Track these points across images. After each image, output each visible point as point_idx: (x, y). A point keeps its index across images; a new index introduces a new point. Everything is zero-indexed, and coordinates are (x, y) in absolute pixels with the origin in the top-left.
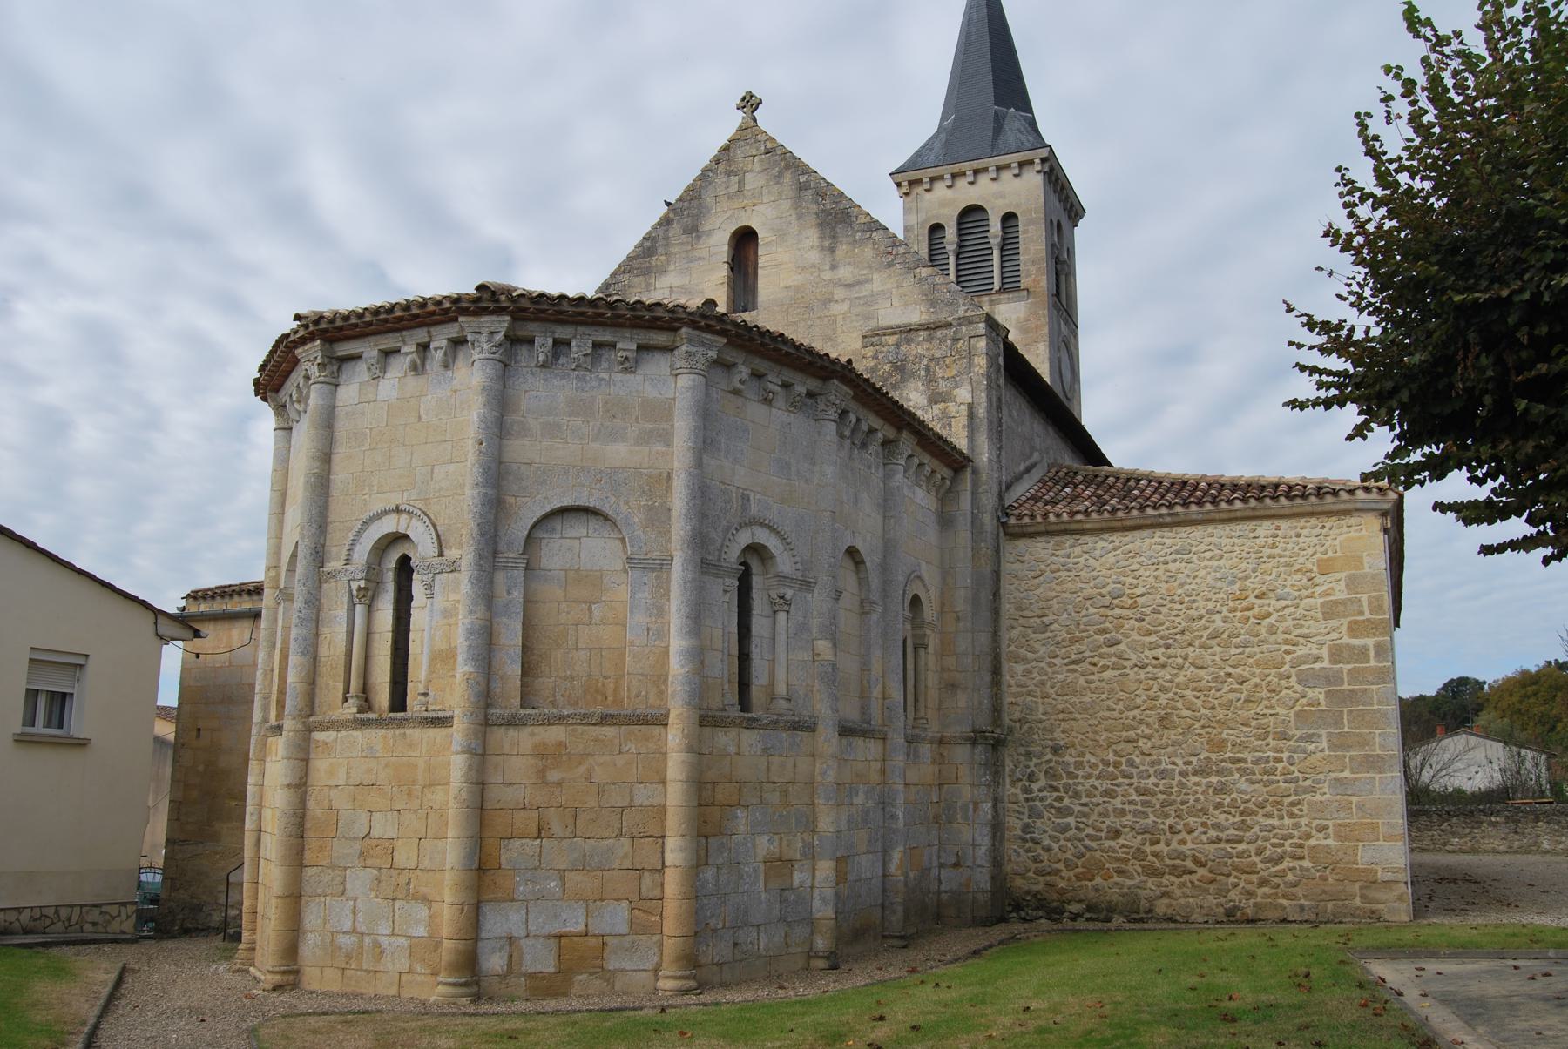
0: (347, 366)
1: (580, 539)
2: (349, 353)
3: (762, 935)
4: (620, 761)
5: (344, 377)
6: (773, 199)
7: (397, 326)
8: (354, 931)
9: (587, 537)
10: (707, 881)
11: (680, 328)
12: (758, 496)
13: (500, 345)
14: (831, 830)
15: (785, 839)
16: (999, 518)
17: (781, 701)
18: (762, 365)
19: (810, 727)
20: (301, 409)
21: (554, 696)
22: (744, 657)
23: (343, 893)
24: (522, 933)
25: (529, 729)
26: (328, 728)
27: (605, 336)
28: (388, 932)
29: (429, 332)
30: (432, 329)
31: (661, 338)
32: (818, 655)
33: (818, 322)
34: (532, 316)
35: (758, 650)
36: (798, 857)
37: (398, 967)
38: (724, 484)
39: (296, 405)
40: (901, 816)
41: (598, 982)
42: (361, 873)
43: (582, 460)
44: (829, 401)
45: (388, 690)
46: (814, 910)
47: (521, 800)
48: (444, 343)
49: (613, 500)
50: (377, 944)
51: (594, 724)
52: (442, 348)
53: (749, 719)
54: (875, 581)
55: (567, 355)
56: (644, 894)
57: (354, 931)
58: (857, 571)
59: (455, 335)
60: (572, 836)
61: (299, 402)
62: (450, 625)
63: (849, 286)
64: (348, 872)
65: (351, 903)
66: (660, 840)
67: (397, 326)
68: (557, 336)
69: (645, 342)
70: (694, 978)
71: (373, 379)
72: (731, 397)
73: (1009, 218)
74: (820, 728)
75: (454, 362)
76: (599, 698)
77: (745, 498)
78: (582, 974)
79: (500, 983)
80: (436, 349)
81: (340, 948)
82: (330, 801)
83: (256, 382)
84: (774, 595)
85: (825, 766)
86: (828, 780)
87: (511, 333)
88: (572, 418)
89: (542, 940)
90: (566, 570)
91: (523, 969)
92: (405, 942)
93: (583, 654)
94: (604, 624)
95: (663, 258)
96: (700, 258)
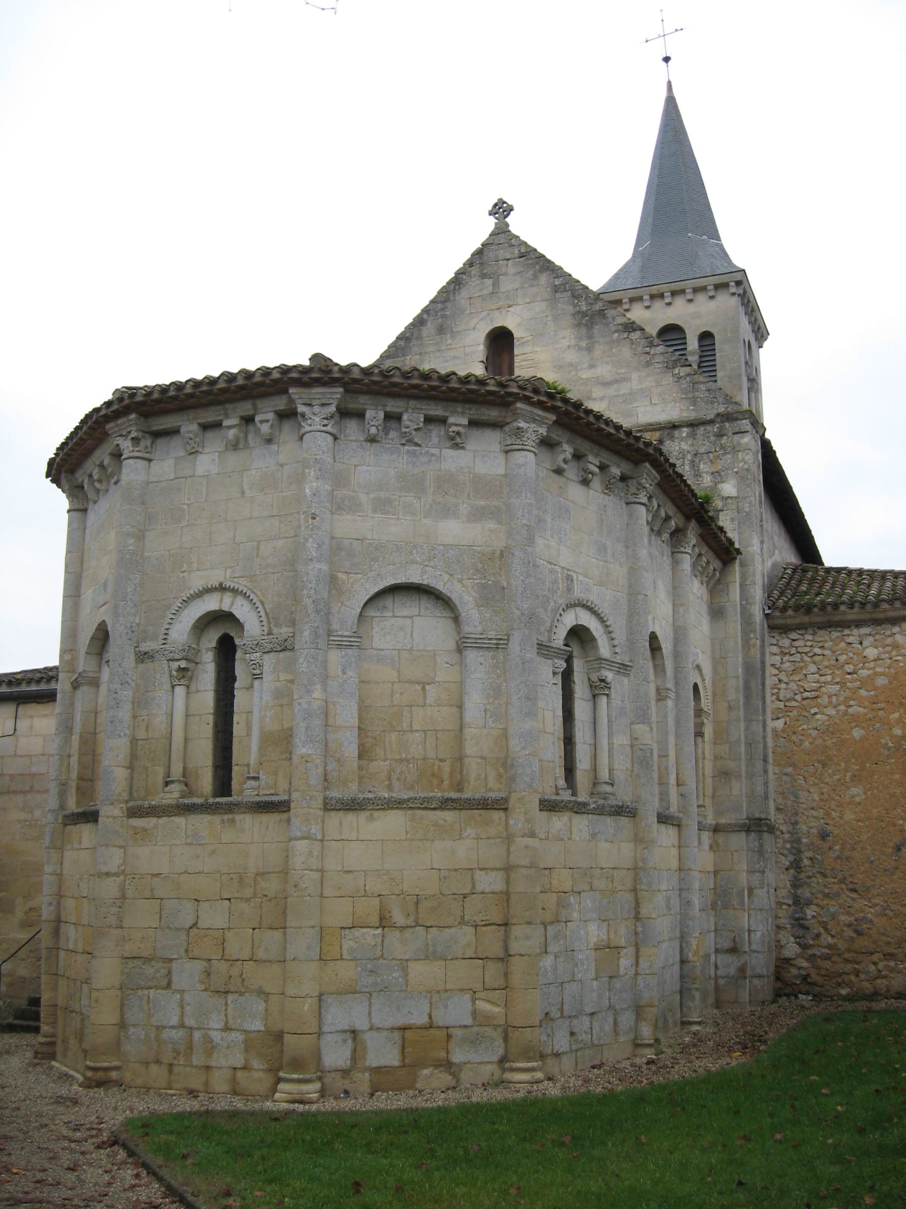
0: (161, 442)
1: (411, 617)
6: (528, 300)
8: (182, 1025)
9: (419, 615)
11: (514, 403)
12: (581, 578)
13: (332, 417)
16: (764, 610)
18: (585, 446)
20: (103, 488)
22: (569, 741)
24: (366, 1027)
25: (368, 813)
28: (220, 1025)
29: (254, 405)
31: (493, 414)
32: (637, 739)
34: (365, 389)
38: (551, 564)
39: (97, 485)
40: (696, 902)
47: (362, 888)
48: (271, 416)
49: (446, 577)
50: (208, 1040)
51: (434, 809)
52: (268, 421)
54: (669, 665)
57: (182, 1025)
58: (654, 657)
59: (282, 407)
60: (413, 924)
61: (100, 481)
62: (282, 706)
63: (607, 384)
64: (174, 965)
65: (179, 996)
66: (502, 928)
67: (221, 398)
68: (388, 409)
69: (476, 417)
72: (555, 477)
73: (706, 337)
76: (435, 781)
80: (262, 422)
83: (51, 463)
84: (594, 678)
87: (342, 405)
90: (398, 650)
91: (368, 1063)
92: (238, 1037)
94: (439, 705)
95: (418, 357)
96: (455, 357)
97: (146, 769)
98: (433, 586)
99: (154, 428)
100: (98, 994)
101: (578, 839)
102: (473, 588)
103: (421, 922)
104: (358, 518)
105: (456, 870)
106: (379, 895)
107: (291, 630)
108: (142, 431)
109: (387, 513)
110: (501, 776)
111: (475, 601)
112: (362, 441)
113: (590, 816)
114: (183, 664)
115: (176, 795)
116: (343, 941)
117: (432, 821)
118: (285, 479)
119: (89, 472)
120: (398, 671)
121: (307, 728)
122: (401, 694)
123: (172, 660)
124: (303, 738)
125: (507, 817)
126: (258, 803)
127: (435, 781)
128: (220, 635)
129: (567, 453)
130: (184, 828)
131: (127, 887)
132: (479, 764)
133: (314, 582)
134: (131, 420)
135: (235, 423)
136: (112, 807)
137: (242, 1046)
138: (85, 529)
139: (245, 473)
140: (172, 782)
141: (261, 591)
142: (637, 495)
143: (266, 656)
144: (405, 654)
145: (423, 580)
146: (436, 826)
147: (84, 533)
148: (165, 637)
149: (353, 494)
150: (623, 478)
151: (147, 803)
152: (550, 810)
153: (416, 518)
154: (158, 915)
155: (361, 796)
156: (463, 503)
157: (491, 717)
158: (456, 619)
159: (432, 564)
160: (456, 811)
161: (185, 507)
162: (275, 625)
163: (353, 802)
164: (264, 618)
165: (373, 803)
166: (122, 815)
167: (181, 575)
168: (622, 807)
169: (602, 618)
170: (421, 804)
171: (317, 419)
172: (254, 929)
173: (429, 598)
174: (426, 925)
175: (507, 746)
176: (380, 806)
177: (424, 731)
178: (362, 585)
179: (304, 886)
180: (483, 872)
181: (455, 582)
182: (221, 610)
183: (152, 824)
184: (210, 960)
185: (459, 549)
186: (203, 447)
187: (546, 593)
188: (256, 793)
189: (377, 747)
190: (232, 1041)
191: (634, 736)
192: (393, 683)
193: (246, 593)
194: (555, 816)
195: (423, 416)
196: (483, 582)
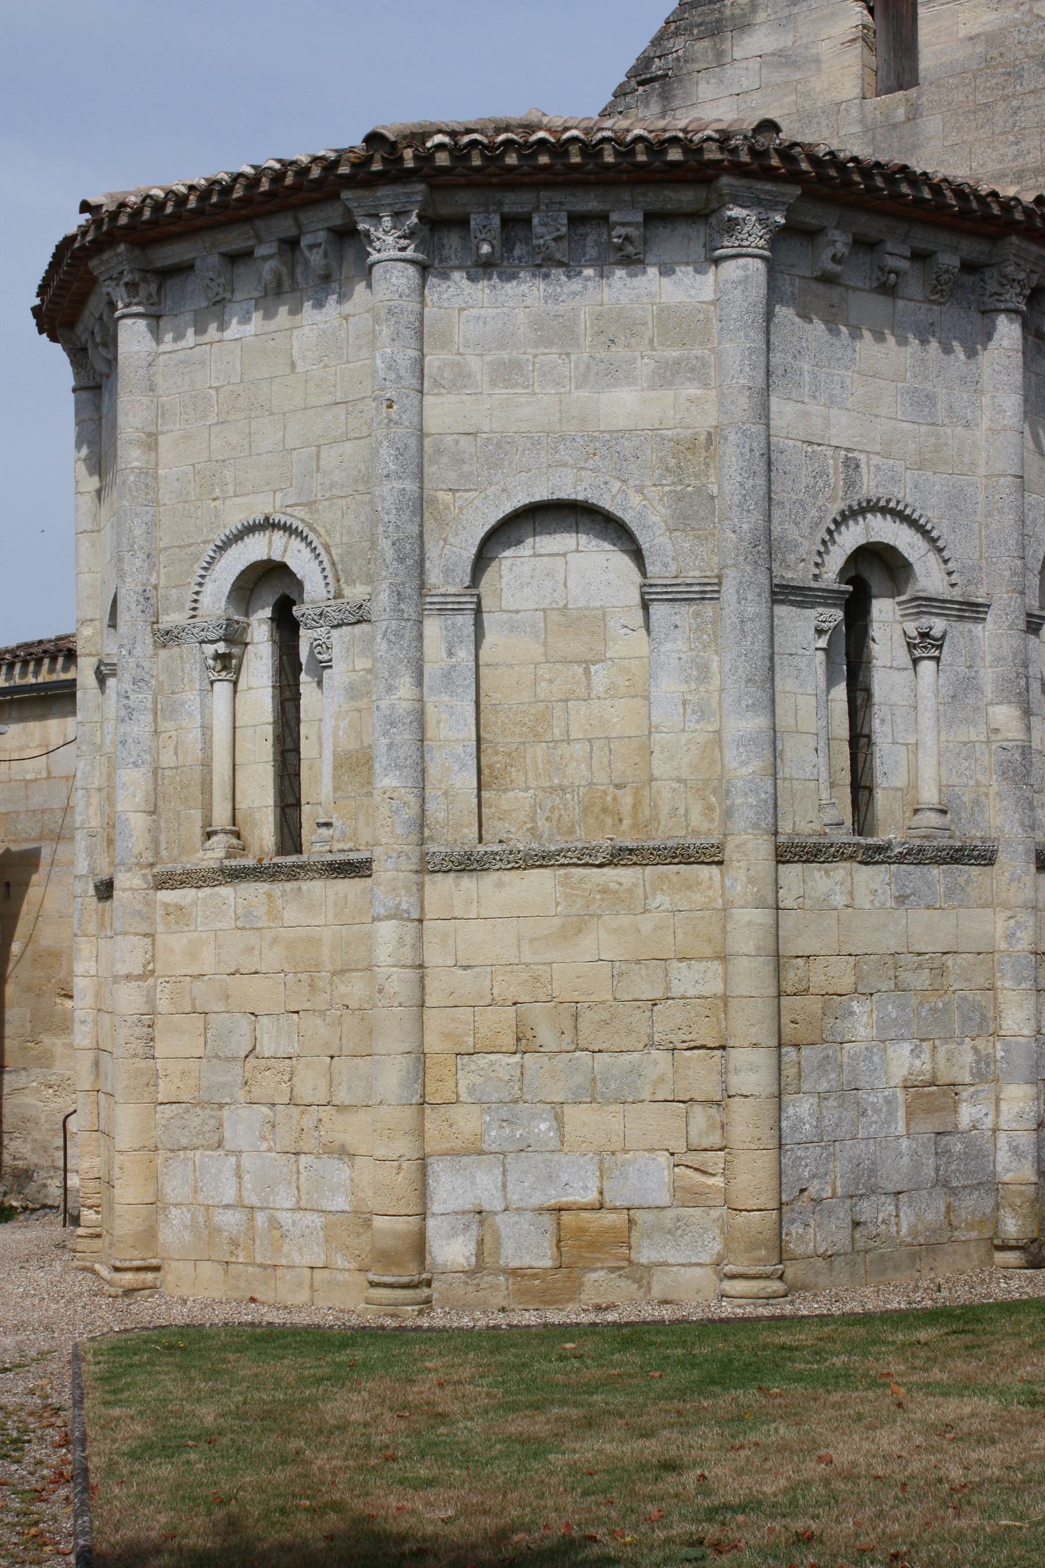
1: (564, 555)
2: (173, 261)
3: (904, 1210)
4: (646, 924)
5: (169, 302)
7: (243, 212)
9: (577, 551)
10: (801, 1121)
11: (716, 177)
12: (876, 460)
14: (1026, 1032)
15: (942, 1050)
17: (928, 813)
18: (872, 226)
19: (986, 858)
21: (533, 820)
23: (220, 1145)
25: (494, 876)
26: (182, 884)
27: (589, 203)
29: (296, 220)
30: (302, 216)
31: (685, 197)
32: (997, 730)
33: (1031, 100)
35: (887, 729)
36: (967, 1080)
37: (308, 1260)
38: (811, 443)
41: (622, 1283)
42: (244, 1112)
43: (560, 421)
44: (1005, 276)
45: (271, 818)
46: (999, 1169)
47: (487, 991)
48: (322, 236)
49: (616, 485)
50: (274, 1224)
51: (601, 866)
52: (319, 245)
53: (868, 848)
55: (527, 241)
56: (695, 1142)
62: (359, 711)
65: (233, 1159)
68: (506, 209)
70: (781, 1278)
71: (215, 303)
72: (820, 288)
74: (1002, 857)
75: (340, 267)
77: (852, 465)
78: (596, 1270)
79: (467, 1284)
80: (311, 247)
81: (219, 1231)
82: (193, 999)
85: (1012, 922)
86: (1020, 947)
87: (430, 212)
88: (541, 350)
89: (529, 1215)
90: (544, 610)
93: (579, 749)
94: (612, 697)
97: (178, 813)
98: (595, 501)
99: (159, 264)
100: (122, 1158)
101: (868, 906)
102: (661, 500)
103: (582, 1044)
104: (468, 398)
105: (638, 962)
106: (515, 1004)
107: (368, 589)
108: (140, 270)
109: (516, 385)
110: (711, 809)
111: (665, 522)
112: (468, 267)
113: (893, 867)
114: (221, 647)
115: (220, 853)
116: (460, 1073)
117: (598, 885)
118: (350, 342)
119: (90, 327)
120: (545, 644)
121: (390, 746)
122: (551, 681)
123: (206, 642)
124: (385, 762)
125: (722, 876)
126: (330, 864)
127: (609, 821)
128: (277, 596)
129: (839, 245)
130: (233, 903)
131: (158, 996)
132: (674, 790)
133: (394, 511)
134: (120, 254)
135: (272, 251)
136: (128, 875)
137: (321, 1234)
138: (100, 418)
139: (295, 333)
140: (215, 833)
141: (324, 527)
142: (1000, 295)
143: (335, 633)
144: (554, 616)
145: (576, 493)
146: (605, 892)
147: (100, 424)
148: (194, 605)
149: (458, 357)
150: (969, 267)
151: (179, 866)
152: (807, 861)
153: (563, 390)
154: (202, 1039)
155: (481, 849)
156: (642, 357)
157: (694, 712)
158: (637, 555)
159: (590, 464)
160: (638, 868)
161: (213, 392)
162: (346, 582)
163: (469, 859)
164: (329, 572)
165: (501, 860)
166: (145, 886)
167: (213, 505)
168: (961, 849)
169: (923, 527)
170: (578, 858)
171: (390, 239)
172: (332, 1057)
173: (593, 521)
174: (591, 1049)
175: (722, 760)
176: (513, 864)
177: (589, 740)
178: (477, 508)
179: (392, 990)
180: (684, 964)
181: (631, 492)
182: (269, 561)
183: (189, 900)
184: (274, 1105)
185: (638, 436)
186: (233, 291)
187: (801, 496)
188: (328, 848)
189: (513, 769)
190: (308, 1227)
191: (992, 727)
192: (536, 665)
193: (302, 532)
194: (819, 870)
195: (565, 214)
196: (679, 488)
